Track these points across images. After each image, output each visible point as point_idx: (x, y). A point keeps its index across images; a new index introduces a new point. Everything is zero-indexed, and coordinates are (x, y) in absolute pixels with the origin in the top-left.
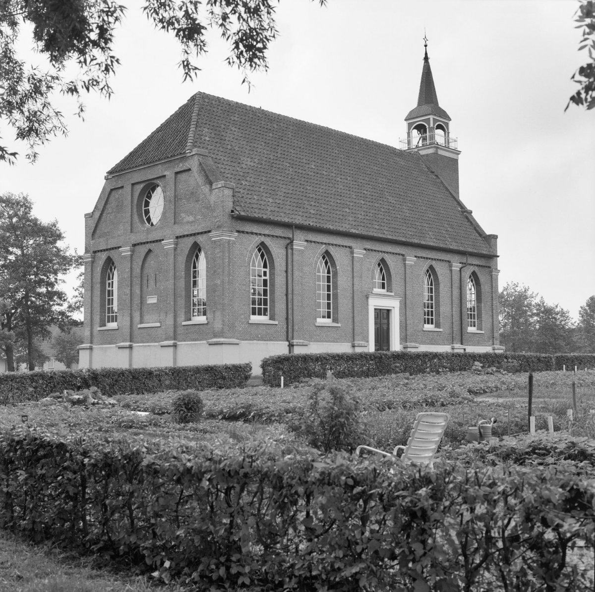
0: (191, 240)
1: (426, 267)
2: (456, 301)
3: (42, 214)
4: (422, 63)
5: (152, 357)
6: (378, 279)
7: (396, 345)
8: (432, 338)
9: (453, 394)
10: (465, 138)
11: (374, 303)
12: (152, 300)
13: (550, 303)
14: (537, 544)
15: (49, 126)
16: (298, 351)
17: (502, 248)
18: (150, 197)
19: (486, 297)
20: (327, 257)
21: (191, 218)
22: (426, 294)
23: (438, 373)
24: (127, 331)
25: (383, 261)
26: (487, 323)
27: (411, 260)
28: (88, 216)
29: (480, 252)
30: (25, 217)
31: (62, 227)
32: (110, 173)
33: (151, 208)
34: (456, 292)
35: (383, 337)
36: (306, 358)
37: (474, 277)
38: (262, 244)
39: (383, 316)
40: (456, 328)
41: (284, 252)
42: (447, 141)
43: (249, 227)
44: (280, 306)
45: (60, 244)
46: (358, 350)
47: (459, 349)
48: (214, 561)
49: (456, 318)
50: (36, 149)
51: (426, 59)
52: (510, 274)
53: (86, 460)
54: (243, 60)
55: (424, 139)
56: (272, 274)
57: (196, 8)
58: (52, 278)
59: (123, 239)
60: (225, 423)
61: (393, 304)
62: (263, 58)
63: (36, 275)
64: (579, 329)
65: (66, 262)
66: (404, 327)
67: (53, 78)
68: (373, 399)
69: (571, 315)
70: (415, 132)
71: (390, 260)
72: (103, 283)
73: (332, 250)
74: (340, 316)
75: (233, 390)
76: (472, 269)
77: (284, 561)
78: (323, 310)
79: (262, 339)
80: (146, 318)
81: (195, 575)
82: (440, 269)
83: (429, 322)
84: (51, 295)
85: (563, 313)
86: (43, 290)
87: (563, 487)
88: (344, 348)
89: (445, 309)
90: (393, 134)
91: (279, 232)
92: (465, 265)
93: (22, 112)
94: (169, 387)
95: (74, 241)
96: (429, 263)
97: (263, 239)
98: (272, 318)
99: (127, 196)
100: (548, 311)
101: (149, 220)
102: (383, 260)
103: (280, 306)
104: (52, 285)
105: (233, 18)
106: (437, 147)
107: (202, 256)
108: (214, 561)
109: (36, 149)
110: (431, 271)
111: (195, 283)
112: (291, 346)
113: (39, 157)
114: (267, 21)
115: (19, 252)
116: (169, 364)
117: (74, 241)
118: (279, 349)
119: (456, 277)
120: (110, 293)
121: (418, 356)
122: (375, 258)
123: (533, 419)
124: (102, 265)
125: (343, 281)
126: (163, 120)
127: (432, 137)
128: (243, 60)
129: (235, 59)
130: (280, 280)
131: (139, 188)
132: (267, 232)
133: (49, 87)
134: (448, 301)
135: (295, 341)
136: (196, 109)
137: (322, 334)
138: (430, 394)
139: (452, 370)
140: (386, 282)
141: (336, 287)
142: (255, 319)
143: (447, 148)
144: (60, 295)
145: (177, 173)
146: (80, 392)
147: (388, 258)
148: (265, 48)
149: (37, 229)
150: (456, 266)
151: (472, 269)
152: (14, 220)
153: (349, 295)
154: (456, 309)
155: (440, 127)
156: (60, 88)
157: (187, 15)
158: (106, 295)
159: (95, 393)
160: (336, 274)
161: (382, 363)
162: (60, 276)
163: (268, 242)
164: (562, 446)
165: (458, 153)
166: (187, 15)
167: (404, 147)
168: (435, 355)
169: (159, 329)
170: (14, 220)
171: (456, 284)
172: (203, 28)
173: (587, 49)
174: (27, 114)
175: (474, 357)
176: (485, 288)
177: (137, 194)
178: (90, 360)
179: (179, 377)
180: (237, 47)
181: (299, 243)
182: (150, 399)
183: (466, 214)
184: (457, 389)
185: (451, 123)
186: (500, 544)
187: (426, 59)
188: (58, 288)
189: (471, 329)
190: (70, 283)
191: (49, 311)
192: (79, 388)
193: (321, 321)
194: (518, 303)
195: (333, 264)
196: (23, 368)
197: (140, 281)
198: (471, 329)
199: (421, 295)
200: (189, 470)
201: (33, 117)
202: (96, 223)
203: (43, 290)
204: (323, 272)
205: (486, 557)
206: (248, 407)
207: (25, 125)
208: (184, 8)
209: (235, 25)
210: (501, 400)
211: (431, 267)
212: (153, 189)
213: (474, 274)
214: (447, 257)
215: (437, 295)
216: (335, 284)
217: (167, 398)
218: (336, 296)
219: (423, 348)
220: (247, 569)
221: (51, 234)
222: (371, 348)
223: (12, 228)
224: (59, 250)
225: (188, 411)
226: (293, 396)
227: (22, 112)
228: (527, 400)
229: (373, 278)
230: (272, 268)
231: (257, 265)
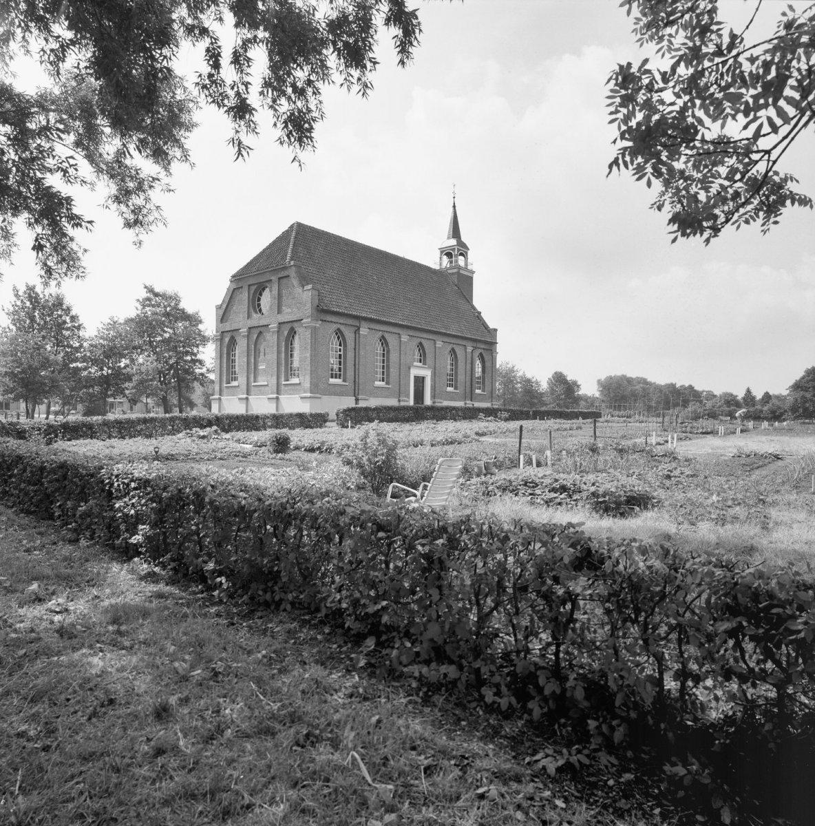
0: (289, 326)
1: (449, 349)
2: (469, 373)
3: (188, 306)
4: (451, 209)
5: (262, 406)
6: (417, 357)
7: (428, 401)
8: (452, 397)
9: (466, 436)
10: (478, 262)
11: (414, 372)
12: (262, 367)
13: (529, 376)
14: (547, 596)
15: (151, 218)
16: (362, 404)
17: (500, 338)
18: (261, 294)
19: (488, 370)
20: (383, 340)
21: (289, 310)
22: (449, 367)
23: (455, 420)
24: (244, 387)
25: (421, 344)
26: (488, 388)
27: (439, 344)
28: (218, 308)
29: (485, 341)
30: (176, 308)
31: (202, 315)
32: (233, 277)
33: (262, 302)
34: (469, 367)
35: (419, 395)
36: (367, 409)
37: (481, 357)
38: (339, 329)
39: (420, 381)
40: (468, 390)
41: (353, 335)
42: (466, 264)
43: (329, 318)
44: (350, 373)
45: (201, 327)
46: (402, 404)
47: (469, 404)
48: (262, 586)
49: (468, 383)
50: (141, 237)
51: (454, 207)
52: (505, 356)
53: (165, 494)
54: (293, 140)
55: (451, 262)
56: (345, 350)
57: (247, 88)
58: (195, 350)
59: (241, 321)
60: (306, 454)
61: (427, 373)
62: (311, 138)
63: (184, 347)
64: (546, 392)
65: (204, 340)
66: (433, 388)
67: (154, 179)
68: (410, 438)
69: (542, 383)
70: (445, 258)
71: (425, 343)
72: (228, 354)
73: (387, 336)
74: (391, 380)
75: (315, 430)
76: (480, 351)
77: (319, 592)
78: (379, 376)
79: (338, 395)
80: (259, 378)
81: (245, 597)
82: (459, 351)
83: (451, 385)
84: (194, 361)
85: (537, 382)
86: (189, 358)
87: (573, 546)
88: (392, 402)
89: (461, 378)
90: (431, 259)
91: (350, 321)
92: (475, 348)
93: (127, 205)
94: (270, 427)
95: (209, 326)
96: (451, 346)
97: (339, 326)
98: (344, 381)
99: (244, 296)
100: (529, 381)
101: (260, 310)
102: (421, 344)
103: (350, 373)
104: (195, 355)
105: (283, 101)
106: (459, 268)
107: (297, 337)
108: (262, 586)
109: (141, 237)
110: (453, 351)
111: (292, 355)
112: (357, 400)
113: (144, 245)
114: (315, 102)
115: (171, 331)
116: (273, 411)
117: (209, 326)
118: (349, 402)
119: (469, 356)
120: (233, 361)
121: (442, 409)
122: (416, 342)
123: (522, 456)
124: (228, 343)
125: (394, 356)
126: (271, 241)
127: (457, 261)
128: (293, 140)
129: (286, 138)
130: (350, 355)
131: (253, 288)
132: (342, 321)
133: (151, 187)
134: (463, 372)
135: (360, 397)
136: (294, 234)
137: (377, 392)
138: (450, 435)
139: (465, 418)
140: (423, 359)
141: (388, 361)
142: (332, 381)
143: (466, 269)
144: (201, 362)
145: (280, 279)
146: (63, 458)
147: (424, 342)
148: (312, 128)
149: (185, 317)
150: (469, 349)
151: (480, 351)
152: (168, 309)
153: (397, 366)
154: (468, 378)
155: (461, 254)
156: (160, 188)
157: (238, 94)
158: (231, 362)
159: (216, 431)
160: (388, 352)
161: (418, 413)
162: (201, 348)
163: (343, 328)
164: (547, 481)
165: (473, 272)
166: (238, 94)
167: (437, 267)
168: (454, 408)
169: (267, 388)
170: (168, 309)
171: (469, 361)
172: (254, 109)
173: (617, 123)
174: (132, 208)
175: (480, 410)
176: (488, 364)
177: (252, 292)
178: (232, 406)
179: (279, 420)
180: (286, 126)
181: (364, 331)
182: (256, 436)
183: (478, 316)
184: (468, 432)
185: (469, 252)
186: (510, 591)
187: (454, 207)
188: (199, 357)
189: (478, 391)
190: (208, 354)
191: (193, 372)
192: (205, 427)
193: (378, 383)
194: (509, 377)
195: (387, 345)
196: (176, 413)
197: (254, 352)
198: (478, 391)
199: (445, 367)
200: (243, 508)
201: (137, 211)
202: (224, 313)
203: (189, 358)
204: (380, 351)
205: (498, 604)
206: (323, 443)
207: (132, 217)
208: (236, 89)
209: (284, 106)
210: (497, 440)
211: (453, 349)
212: (264, 289)
213: (481, 354)
214: (464, 343)
215: (456, 368)
216: (388, 359)
217: (266, 435)
218: (388, 366)
219: (446, 403)
220: (290, 597)
221: (193, 320)
222: (411, 403)
223: (167, 315)
224: (200, 331)
225: (281, 445)
226: (353, 435)
227: (127, 205)
228: (518, 440)
229: (414, 355)
230: (345, 346)
231: (335, 344)
